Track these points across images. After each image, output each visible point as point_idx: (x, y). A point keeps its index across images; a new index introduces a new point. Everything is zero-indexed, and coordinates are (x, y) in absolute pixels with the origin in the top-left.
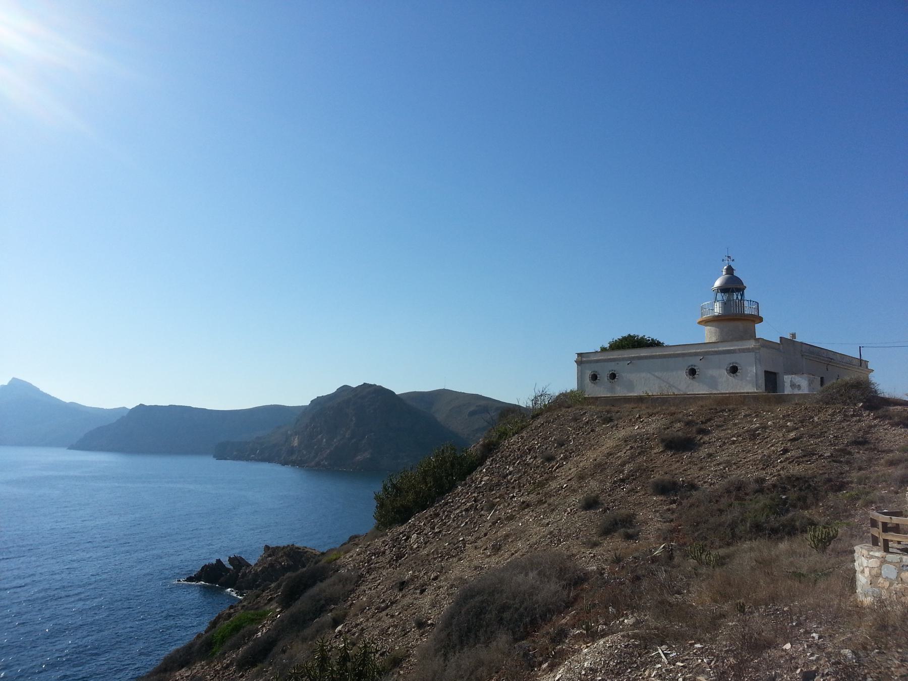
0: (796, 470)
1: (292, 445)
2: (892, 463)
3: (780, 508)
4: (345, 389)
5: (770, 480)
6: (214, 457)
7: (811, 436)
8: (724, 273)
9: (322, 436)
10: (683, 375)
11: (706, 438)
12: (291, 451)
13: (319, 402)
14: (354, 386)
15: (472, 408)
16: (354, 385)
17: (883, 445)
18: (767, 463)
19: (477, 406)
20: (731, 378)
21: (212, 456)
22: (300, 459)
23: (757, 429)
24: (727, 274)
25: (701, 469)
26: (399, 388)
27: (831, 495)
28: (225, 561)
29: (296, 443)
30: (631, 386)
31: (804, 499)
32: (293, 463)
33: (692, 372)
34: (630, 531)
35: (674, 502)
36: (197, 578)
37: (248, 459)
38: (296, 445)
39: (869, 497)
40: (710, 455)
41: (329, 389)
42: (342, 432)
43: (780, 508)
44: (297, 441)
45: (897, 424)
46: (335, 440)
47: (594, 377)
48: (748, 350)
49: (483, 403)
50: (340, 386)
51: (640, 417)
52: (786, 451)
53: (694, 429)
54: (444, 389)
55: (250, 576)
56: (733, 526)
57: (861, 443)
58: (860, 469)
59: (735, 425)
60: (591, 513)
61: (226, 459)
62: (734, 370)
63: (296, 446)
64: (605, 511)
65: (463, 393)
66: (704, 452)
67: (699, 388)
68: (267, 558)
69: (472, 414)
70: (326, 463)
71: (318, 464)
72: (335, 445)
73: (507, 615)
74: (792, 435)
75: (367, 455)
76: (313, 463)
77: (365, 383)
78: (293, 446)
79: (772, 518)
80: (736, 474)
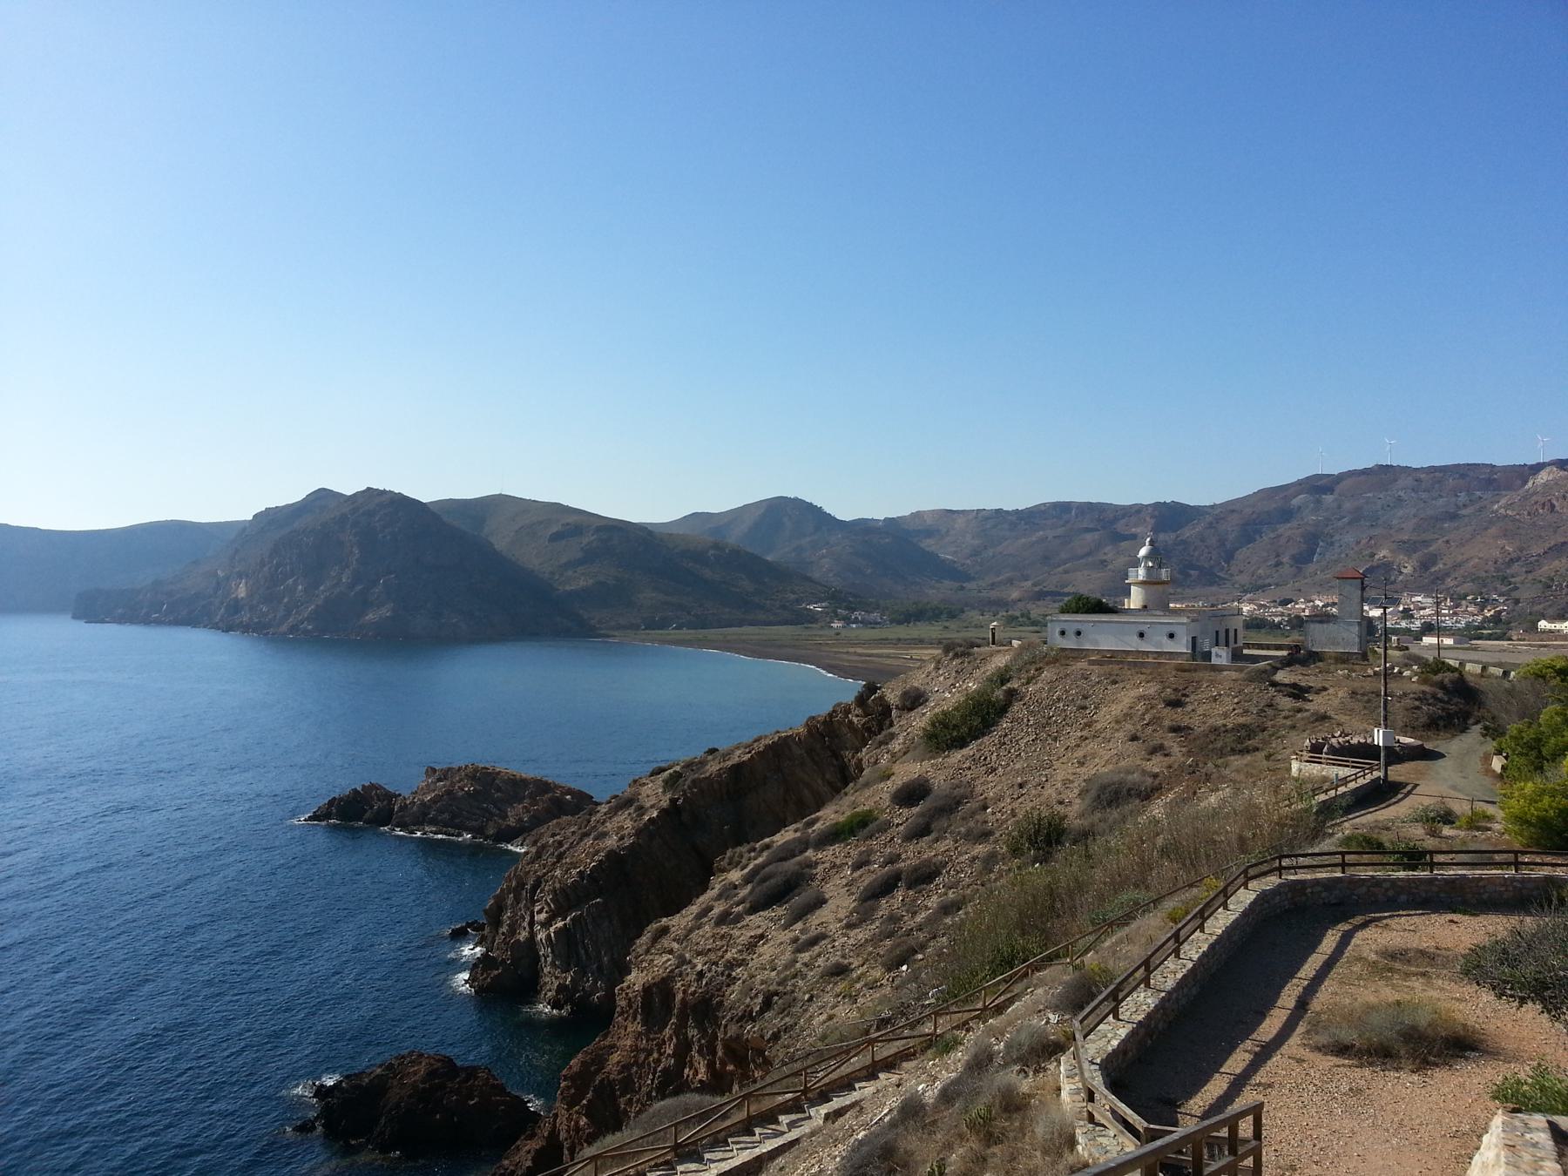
0: (1241, 720)
1: (234, 596)
2: (1285, 718)
3: (1240, 740)
4: (322, 498)
5: (1230, 726)
6: (75, 617)
7: (1245, 701)
8: (1147, 544)
9: (294, 581)
10: (1136, 638)
11: (1188, 700)
12: (236, 607)
13: (270, 519)
14: (349, 492)
15: (555, 529)
16: (348, 487)
17: (1280, 707)
18: (1225, 715)
19: (563, 525)
20: (1169, 642)
21: (70, 616)
22: (256, 620)
23: (1216, 696)
24: (1150, 545)
25: (1190, 718)
26: (426, 491)
27: (1260, 734)
28: (359, 789)
29: (242, 592)
30: (1097, 643)
31: (1249, 735)
32: (245, 629)
33: (1141, 635)
34: (1166, 752)
35: (1182, 736)
36: (327, 816)
37: (146, 621)
38: (242, 595)
39: (1278, 735)
40: (1193, 710)
41: (291, 492)
42: (332, 574)
43: (1240, 740)
44: (244, 589)
45: (1285, 696)
46: (322, 588)
47: (1063, 633)
48: (1183, 624)
49: (571, 519)
50: (309, 493)
51: (1140, 683)
52: (1234, 710)
53: (1180, 694)
54: (500, 495)
55: (415, 808)
56: (1221, 749)
57: (1270, 706)
58: (1271, 720)
59: (1202, 691)
60: (1464, 780)
61: (103, 622)
62: (1171, 636)
63: (242, 598)
64: (1144, 741)
65: (534, 501)
66: (1189, 708)
67: (1145, 647)
68: (436, 783)
69: (556, 537)
70: (310, 627)
71: (293, 629)
72: (322, 597)
73: (1132, 792)
74: (1236, 700)
75: (386, 612)
76: (284, 628)
77: (369, 489)
78: (237, 597)
79: (1238, 746)
80: (1211, 721)
